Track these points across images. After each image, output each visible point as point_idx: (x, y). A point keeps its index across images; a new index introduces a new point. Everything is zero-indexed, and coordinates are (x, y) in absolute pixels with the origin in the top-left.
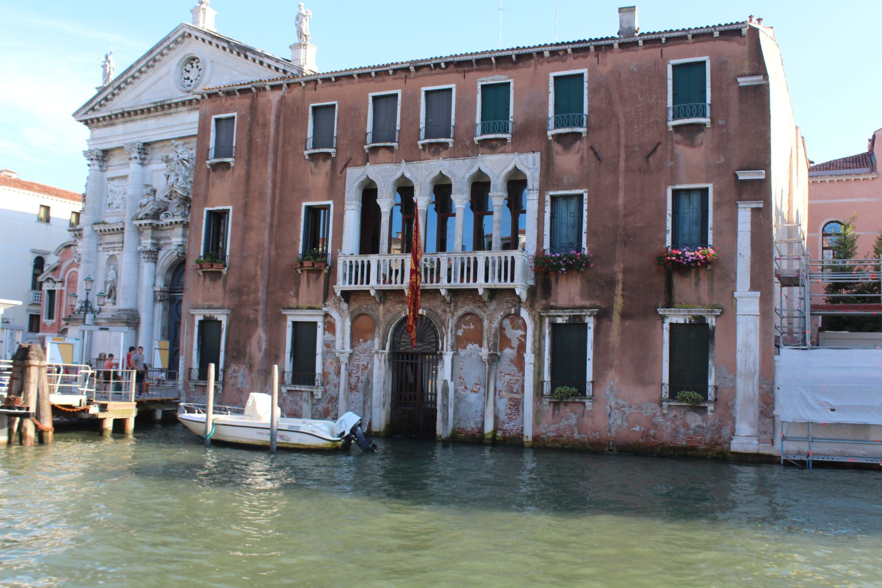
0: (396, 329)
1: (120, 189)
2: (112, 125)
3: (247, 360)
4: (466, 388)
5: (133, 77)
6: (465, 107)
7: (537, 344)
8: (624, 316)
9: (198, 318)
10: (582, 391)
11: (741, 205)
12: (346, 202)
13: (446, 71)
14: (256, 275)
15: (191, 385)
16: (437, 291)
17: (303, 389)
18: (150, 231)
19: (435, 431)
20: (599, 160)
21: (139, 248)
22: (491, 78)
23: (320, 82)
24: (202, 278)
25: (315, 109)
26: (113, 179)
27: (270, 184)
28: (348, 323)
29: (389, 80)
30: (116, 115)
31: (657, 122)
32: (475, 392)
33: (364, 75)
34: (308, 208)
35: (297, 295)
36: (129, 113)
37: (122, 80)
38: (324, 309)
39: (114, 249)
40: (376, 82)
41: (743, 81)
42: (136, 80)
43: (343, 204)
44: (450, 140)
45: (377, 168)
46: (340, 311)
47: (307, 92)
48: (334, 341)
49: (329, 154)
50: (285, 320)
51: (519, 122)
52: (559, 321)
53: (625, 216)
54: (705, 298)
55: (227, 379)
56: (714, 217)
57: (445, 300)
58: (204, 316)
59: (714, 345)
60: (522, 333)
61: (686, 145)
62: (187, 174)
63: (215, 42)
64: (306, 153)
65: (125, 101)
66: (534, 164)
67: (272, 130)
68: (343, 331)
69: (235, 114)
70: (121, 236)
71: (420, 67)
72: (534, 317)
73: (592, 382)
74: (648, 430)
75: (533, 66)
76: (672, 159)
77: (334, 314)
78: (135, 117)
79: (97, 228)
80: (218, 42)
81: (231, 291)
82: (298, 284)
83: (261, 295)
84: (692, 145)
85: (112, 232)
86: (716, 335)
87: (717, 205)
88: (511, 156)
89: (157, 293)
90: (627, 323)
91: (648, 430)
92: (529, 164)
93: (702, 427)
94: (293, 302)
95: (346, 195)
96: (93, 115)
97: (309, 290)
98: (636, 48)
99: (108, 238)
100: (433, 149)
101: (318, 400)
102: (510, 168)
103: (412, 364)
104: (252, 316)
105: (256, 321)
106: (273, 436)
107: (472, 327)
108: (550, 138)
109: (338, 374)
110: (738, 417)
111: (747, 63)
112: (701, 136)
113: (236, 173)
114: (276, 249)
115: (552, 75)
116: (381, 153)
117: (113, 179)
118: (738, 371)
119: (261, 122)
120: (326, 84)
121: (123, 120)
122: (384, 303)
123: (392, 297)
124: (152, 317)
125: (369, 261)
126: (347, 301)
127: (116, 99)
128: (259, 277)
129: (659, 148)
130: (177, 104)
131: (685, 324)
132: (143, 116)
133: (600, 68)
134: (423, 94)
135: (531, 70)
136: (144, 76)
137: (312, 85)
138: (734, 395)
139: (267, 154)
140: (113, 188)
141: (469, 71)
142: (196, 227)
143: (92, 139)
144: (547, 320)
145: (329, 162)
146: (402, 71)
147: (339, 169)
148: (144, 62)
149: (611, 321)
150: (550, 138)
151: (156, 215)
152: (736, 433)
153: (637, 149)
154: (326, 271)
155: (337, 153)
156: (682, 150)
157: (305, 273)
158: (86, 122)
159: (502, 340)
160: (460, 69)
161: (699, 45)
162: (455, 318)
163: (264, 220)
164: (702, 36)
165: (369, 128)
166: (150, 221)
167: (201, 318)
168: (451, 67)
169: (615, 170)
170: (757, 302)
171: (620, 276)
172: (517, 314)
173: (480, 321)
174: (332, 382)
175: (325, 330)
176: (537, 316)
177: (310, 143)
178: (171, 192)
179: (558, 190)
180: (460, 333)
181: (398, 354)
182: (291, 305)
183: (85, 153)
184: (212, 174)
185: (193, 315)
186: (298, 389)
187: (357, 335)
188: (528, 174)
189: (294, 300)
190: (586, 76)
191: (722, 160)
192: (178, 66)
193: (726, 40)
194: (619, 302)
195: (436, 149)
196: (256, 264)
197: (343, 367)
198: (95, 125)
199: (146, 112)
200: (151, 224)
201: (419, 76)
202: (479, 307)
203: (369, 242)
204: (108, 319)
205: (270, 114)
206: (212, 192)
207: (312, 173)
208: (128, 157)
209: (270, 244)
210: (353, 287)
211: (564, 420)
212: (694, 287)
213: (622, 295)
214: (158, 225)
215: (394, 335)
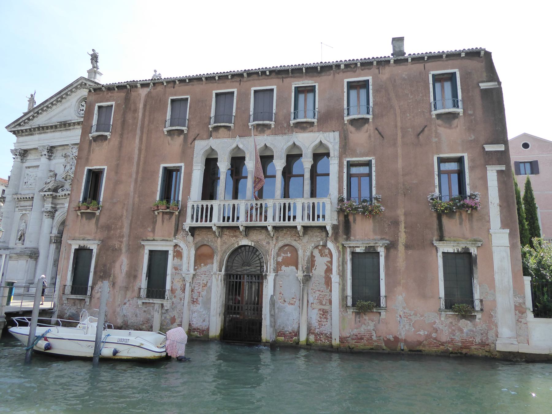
0: (230, 257)
1: (34, 173)
2: (32, 135)
3: (111, 279)
4: (284, 301)
5: (47, 107)
6: (282, 100)
7: (341, 268)
8: (407, 247)
9: (75, 246)
10: (378, 305)
11: (489, 168)
12: (194, 164)
13: (270, 77)
14: (122, 215)
15: (64, 298)
17: (154, 302)
18: (51, 199)
20: (383, 137)
21: (43, 209)
22: (302, 82)
23: (177, 83)
24: (80, 217)
25: (173, 101)
26: (29, 167)
27: (136, 151)
28: (193, 252)
29: (228, 83)
30: (34, 129)
31: (423, 112)
32: (292, 304)
33: (210, 78)
34: (165, 169)
35: (153, 231)
36: (43, 128)
37: (40, 108)
38: (174, 241)
39: (26, 210)
40: (218, 83)
41: (483, 86)
42: (49, 109)
44: (272, 123)
45: (218, 141)
46: (186, 242)
48: (181, 265)
49: (183, 131)
50: (144, 248)
52: (358, 250)
54: (468, 234)
57: (269, 234)
58: (79, 246)
59: (477, 268)
60: (329, 259)
64: (165, 130)
65: (41, 120)
66: (335, 139)
67: (140, 114)
68: (189, 258)
69: (113, 103)
70: (31, 202)
71: (251, 74)
73: (386, 297)
74: (431, 334)
75: (332, 75)
77: (182, 245)
78: (47, 131)
79: (15, 196)
81: (102, 227)
82: (154, 223)
83: (126, 230)
84: (450, 127)
85: (25, 199)
87: (471, 168)
88: (317, 134)
89: (52, 238)
90: (410, 252)
91: (431, 334)
92: (331, 140)
93: (472, 331)
94: (150, 236)
95: (194, 159)
96: (18, 128)
97: (164, 226)
98: (406, 63)
99: (23, 203)
100: (259, 129)
101: (167, 310)
102: (317, 142)
103: (259, 283)
105: (120, 249)
107: (289, 255)
108: (346, 122)
109: (184, 290)
110: (499, 324)
112: (455, 122)
113: (112, 143)
114: (139, 197)
115: (346, 81)
116: (222, 130)
117: (29, 167)
118: (497, 288)
121: (38, 132)
122: (221, 237)
123: (227, 233)
124: (47, 251)
125: (212, 206)
126: (193, 235)
127: (35, 119)
128: (124, 217)
129: (426, 129)
130: (74, 123)
131: (454, 253)
132: (52, 130)
133: (380, 76)
134: (252, 92)
135: (331, 77)
136: (54, 107)
137: (172, 85)
140: (28, 173)
141: (286, 78)
142: (78, 180)
143: (18, 142)
144: (348, 250)
145: (182, 137)
146: (238, 76)
147: (190, 141)
148: (55, 98)
150: (346, 122)
151: (55, 190)
153: (410, 130)
154: (177, 213)
155: (188, 131)
156: (442, 131)
157: (161, 214)
158: (14, 132)
160: (280, 76)
161: (450, 62)
162: (277, 248)
163: (131, 176)
164: (454, 56)
165: (213, 114)
166: (51, 193)
167: (77, 247)
168: (274, 74)
169: (395, 144)
170: (507, 236)
171: (402, 218)
172: (325, 246)
173: (296, 250)
175: (174, 257)
176: (341, 247)
177: (168, 123)
178: (67, 176)
179: (353, 157)
180: (280, 259)
181: (230, 275)
182: (148, 238)
183: (12, 151)
184: (94, 144)
185: (71, 245)
188: (330, 146)
189: (151, 234)
191: (473, 137)
192: (77, 102)
193: (470, 59)
194: (402, 238)
195: (262, 128)
196: (123, 208)
197: (188, 285)
198: (20, 134)
199: (54, 128)
200: (51, 195)
201: (249, 80)
202: (295, 240)
203: (209, 193)
204: (16, 254)
205: (140, 103)
206: (92, 156)
207: (169, 144)
208: (40, 154)
209: (135, 192)
210: (199, 224)
211: (363, 326)
212: (458, 225)
213: (405, 232)
214: (56, 196)
215: (228, 261)
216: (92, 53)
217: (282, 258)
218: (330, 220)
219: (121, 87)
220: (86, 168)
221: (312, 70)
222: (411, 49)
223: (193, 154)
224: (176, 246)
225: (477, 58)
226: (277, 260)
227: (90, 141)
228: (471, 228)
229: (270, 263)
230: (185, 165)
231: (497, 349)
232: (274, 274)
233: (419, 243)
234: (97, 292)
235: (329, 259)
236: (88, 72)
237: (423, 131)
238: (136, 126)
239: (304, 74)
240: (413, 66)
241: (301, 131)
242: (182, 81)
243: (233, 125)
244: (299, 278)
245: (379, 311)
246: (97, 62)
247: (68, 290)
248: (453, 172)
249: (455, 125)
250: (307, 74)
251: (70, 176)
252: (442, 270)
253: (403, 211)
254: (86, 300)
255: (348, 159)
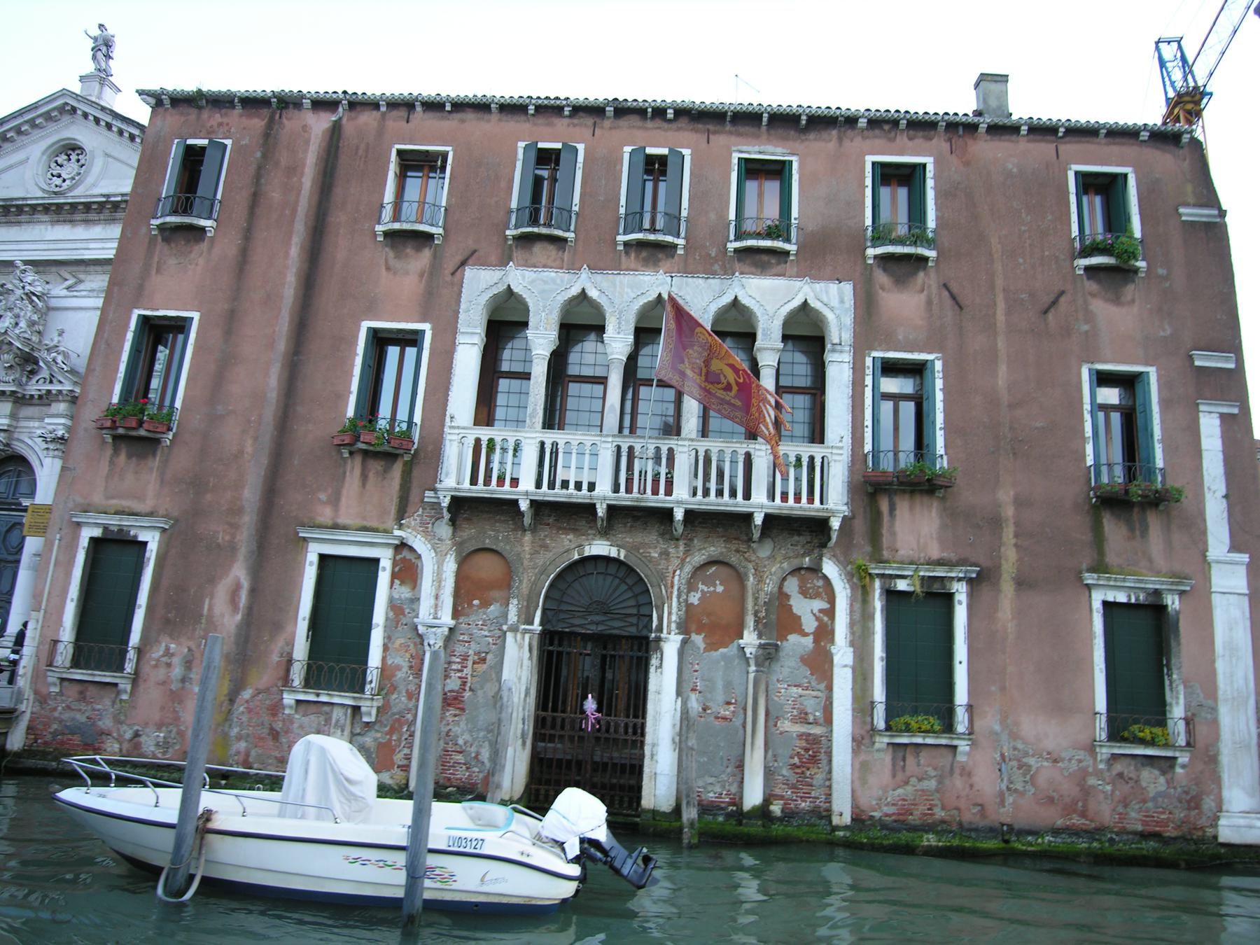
8: (1022, 583)
13: (674, 126)
14: (241, 452)
16: (667, 514)
19: (639, 798)
20: (961, 308)
22: (757, 148)
23: (419, 109)
28: (450, 566)
31: (1057, 257)
35: (335, 501)
38: (397, 533)
43: (455, 332)
46: (428, 534)
47: (390, 124)
51: (811, 227)
52: (902, 585)
53: (1011, 406)
55: (146, 669)
56: (1162, 421)
59: (1179, 644)
60: (825, 606)
61: (1107, 300)
62: (35, 317)
63: (117, 124)
66: (842, 301)
68: (438, 581)
71: (623, 110)
72: (850, 576)
76: (1087, 322)
77: (420, 544)
80: (124, 127)
84: (1117, 301)
86: (1181, 624)
87: (1165, 404)
88: (797, 284)
92: (834, 302)
95: (461, 316)
98: (1014, 137)
102: (797, 303)
104: (223, 538)
105: (233, 548)
106: (415, 874)
107: (720, 589)
111: (1189, 188)
113: (217, 251)
115: (870, 159)
116: (538, 248)
118: (1220, 693)
119: (283, 162)
120: (430, 115)
126: (453, 522)
129: (1062, 299)
138: (1217, 737)
139: (292, 221)
141: (715, 133)
144: (877, 583)
145: (427, 254)
146: (591, 111)
147: (450, 265)
149: (999, 591)
150: (870, 261)
152: (1224, 808)
155: (445, 237)
156: (1101, 308)
159: (779, 621)
160: (700, 126)
162: (688, 569)
167: (97, 532)
169: (991, 328)
171: (1009, 512)
172: (816, 570)
173: (741, 578)
174: (402, 688)
175: (394, 576)
180: (695, 599)
182: (320, 520)
184: (160, 245)
186: (324, 699)
187: (467, 593)
190: (930, 169)
192: (43, 154)
195: (652, 252)
202: (737, 551)
205: (306, 151)
206: (155, 280)
207: (388, 268)
213: (1016, 545)
216: (97, 32)
217: (699, 595)
218: (836, 501)
219: (253, 103)
220: (137, 313)
221: (785, 122)
222: (1024, 105)
223: (458, 302)
224: (402, 546)
225: (1172, 148)
226: (686, 601)
227: (152, 240)
228: (1169, 544)
229: (670, 607)
230: (433, 329)
231: (1221, 840)
232: (681, 637)
233: (1055, 577)
234: (156, 666)
235: (825, 606)
236: (83, 79)
237: (1054, 303)
238: (294, 211)
239: (764, 128)
240: (1031, 146)
241: (753, 270)
242: (434, 106)
243: (573, 235)
244: (748, 651)
245: (955, 742)
246: (108, 57)
247: (65, 653)
248: (1113, 408)
249: (1129, 298)
250: (772, 132)
251: (10, 343)
252: (1102, 645)
253: (1012, 493)
254: (121, 686)
255: (938, 365)
